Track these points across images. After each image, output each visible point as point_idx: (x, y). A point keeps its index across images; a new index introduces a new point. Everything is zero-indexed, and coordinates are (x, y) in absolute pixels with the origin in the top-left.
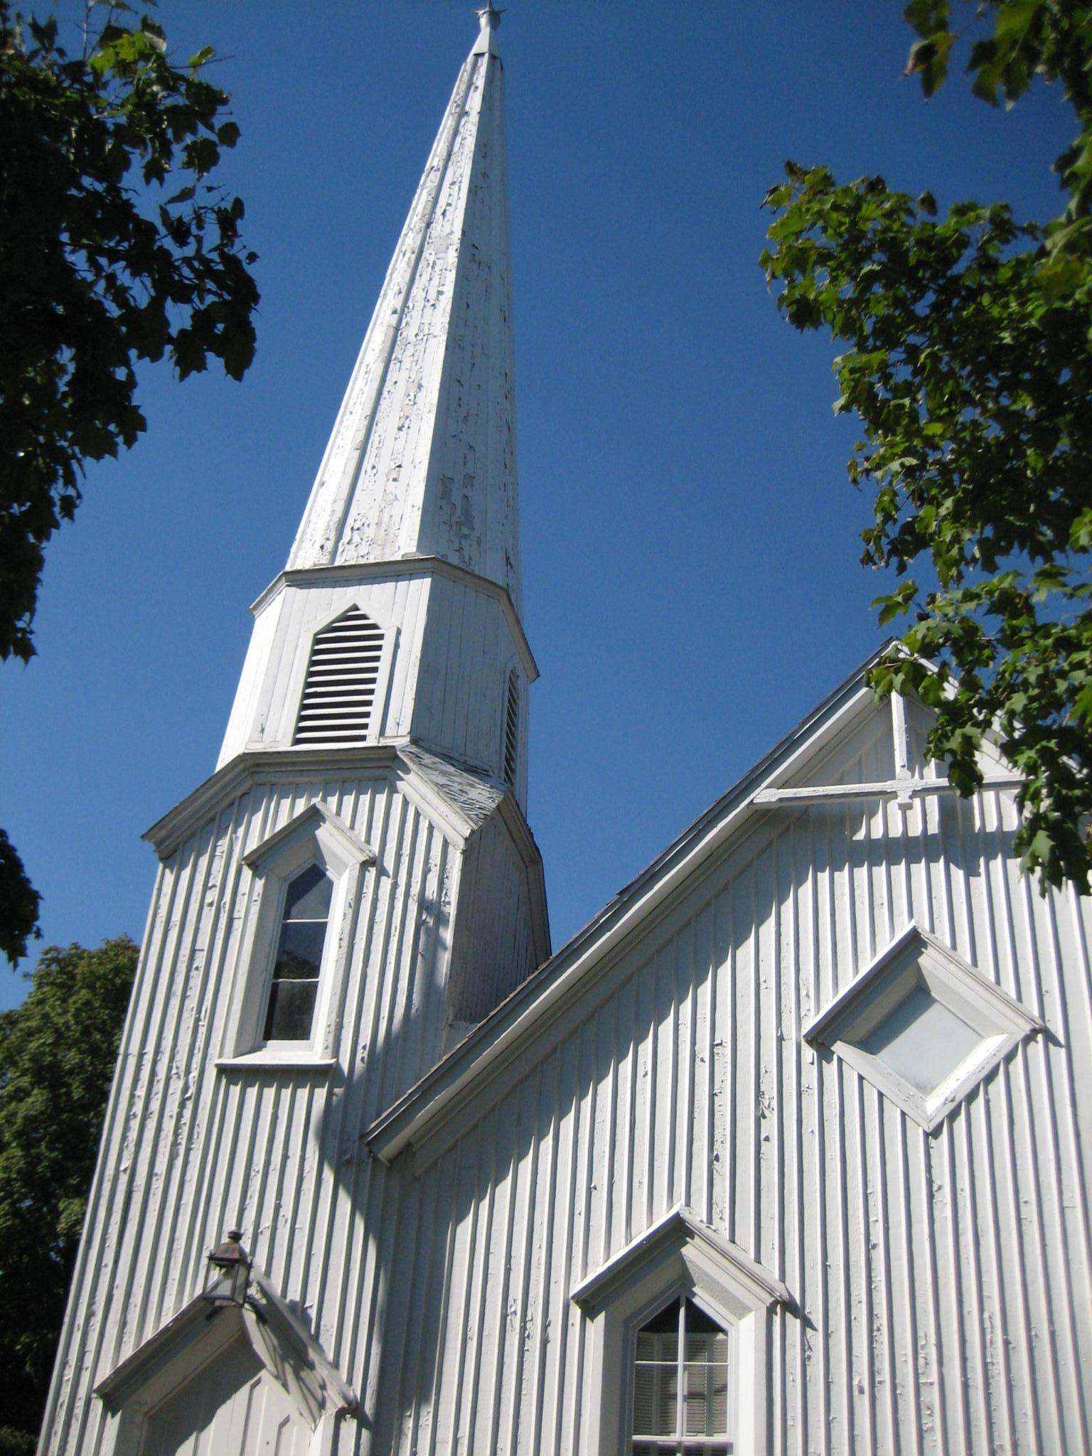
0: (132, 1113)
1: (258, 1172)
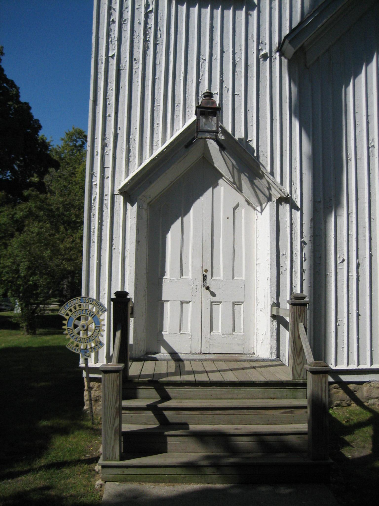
0: (111, 20)
1: (205, 60)
